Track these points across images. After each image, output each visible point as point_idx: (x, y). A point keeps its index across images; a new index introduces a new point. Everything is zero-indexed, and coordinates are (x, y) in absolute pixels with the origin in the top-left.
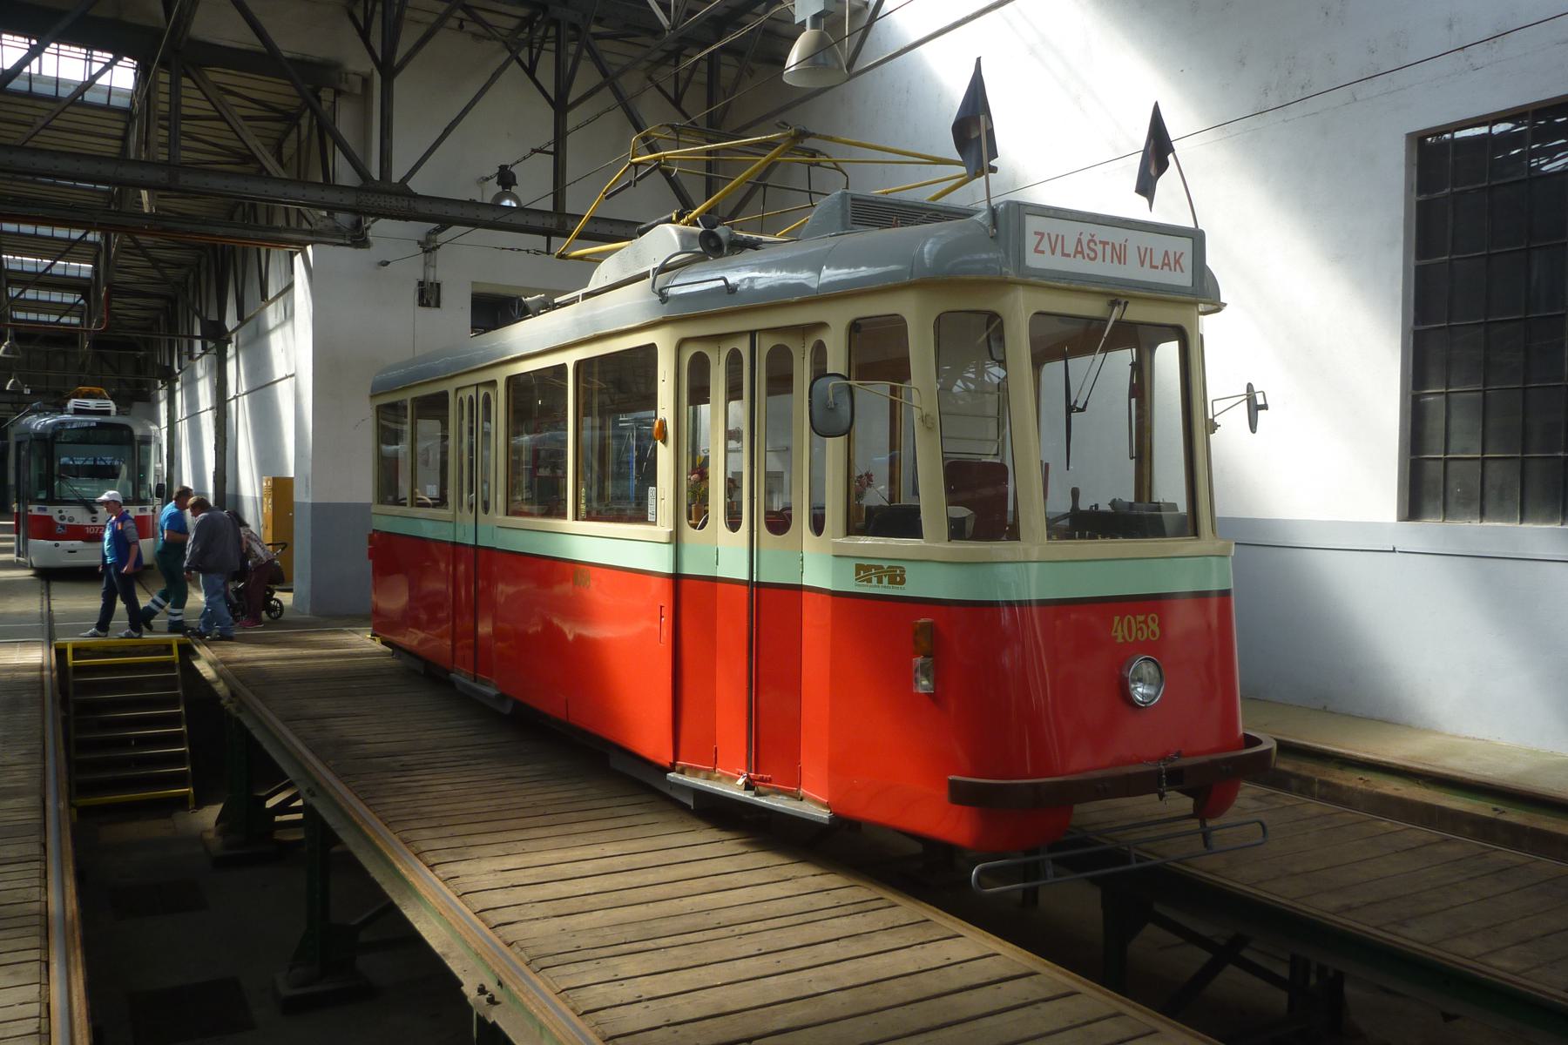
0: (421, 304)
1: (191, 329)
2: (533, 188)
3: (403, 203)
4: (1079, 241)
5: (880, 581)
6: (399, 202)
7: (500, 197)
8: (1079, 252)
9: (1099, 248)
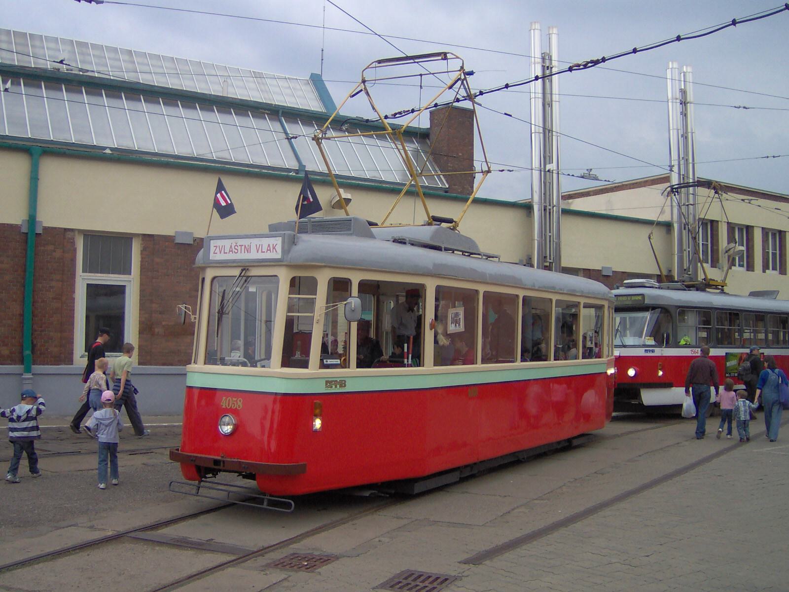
4: (231, 246)
5: (336, 387)
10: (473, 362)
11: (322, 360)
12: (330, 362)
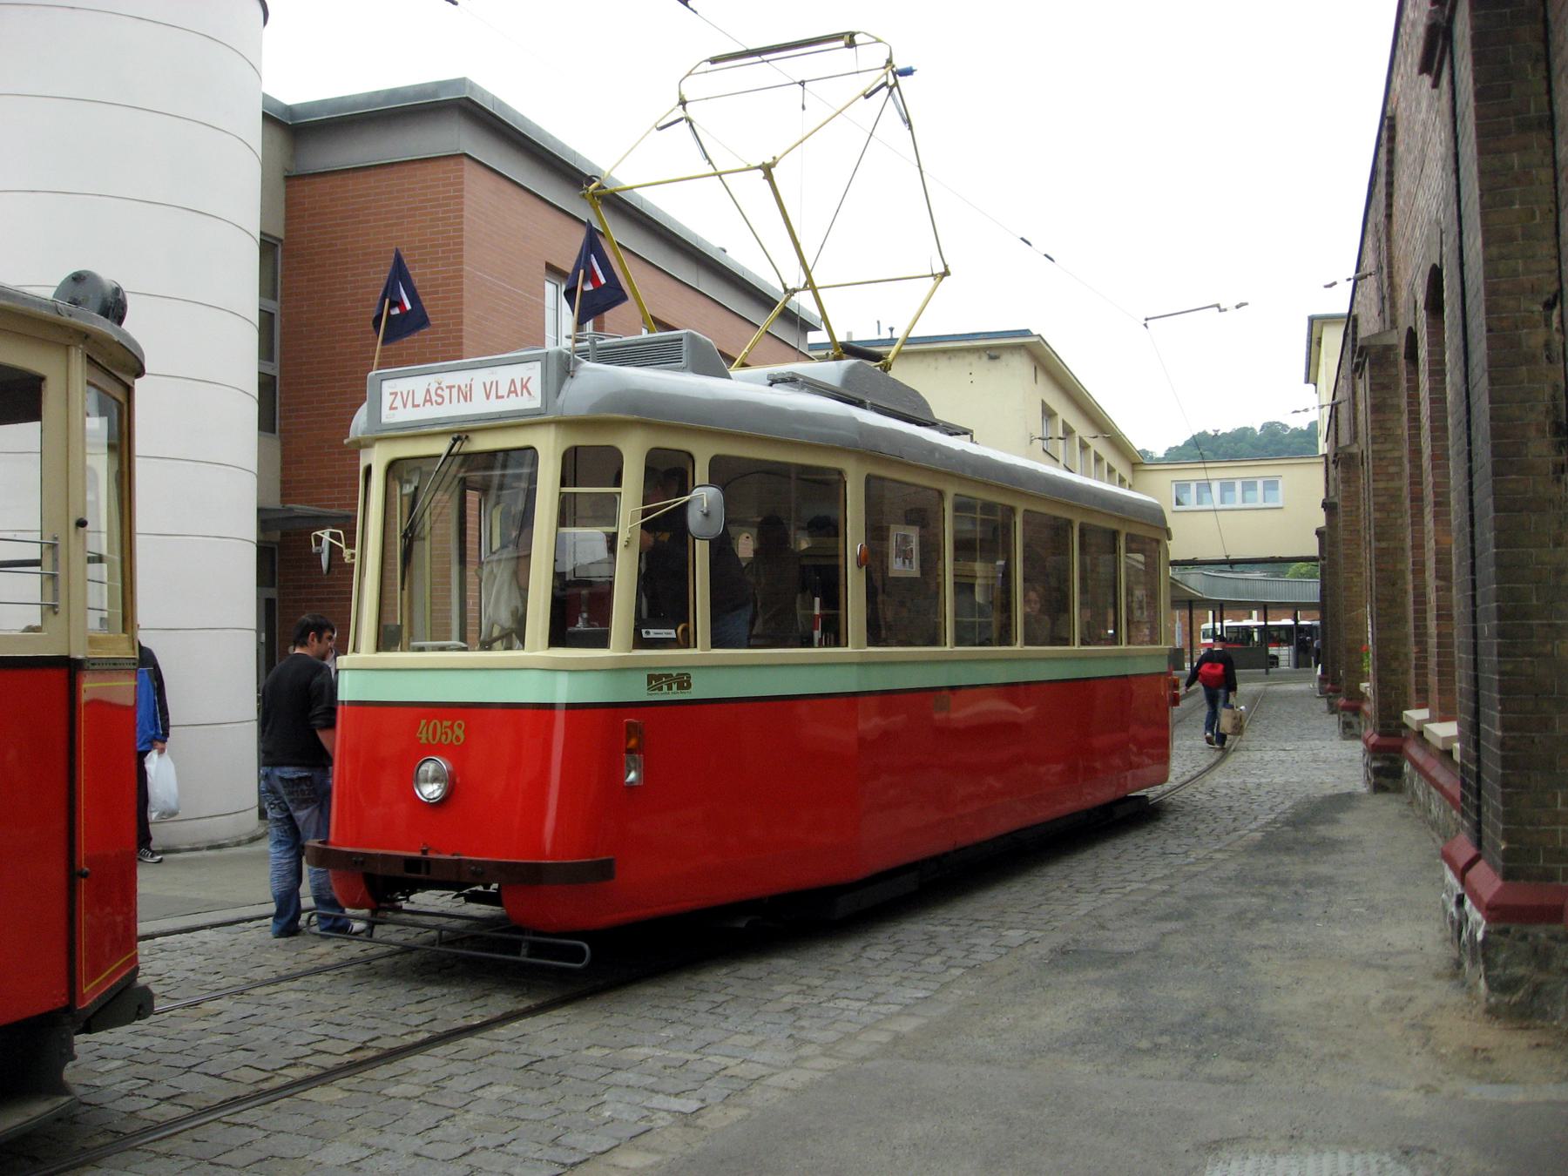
5: (670, 688)
8: (512, 391)
9: (446, 394)
10: (934, 639)
11: (637, 631)
12: (654, 633)
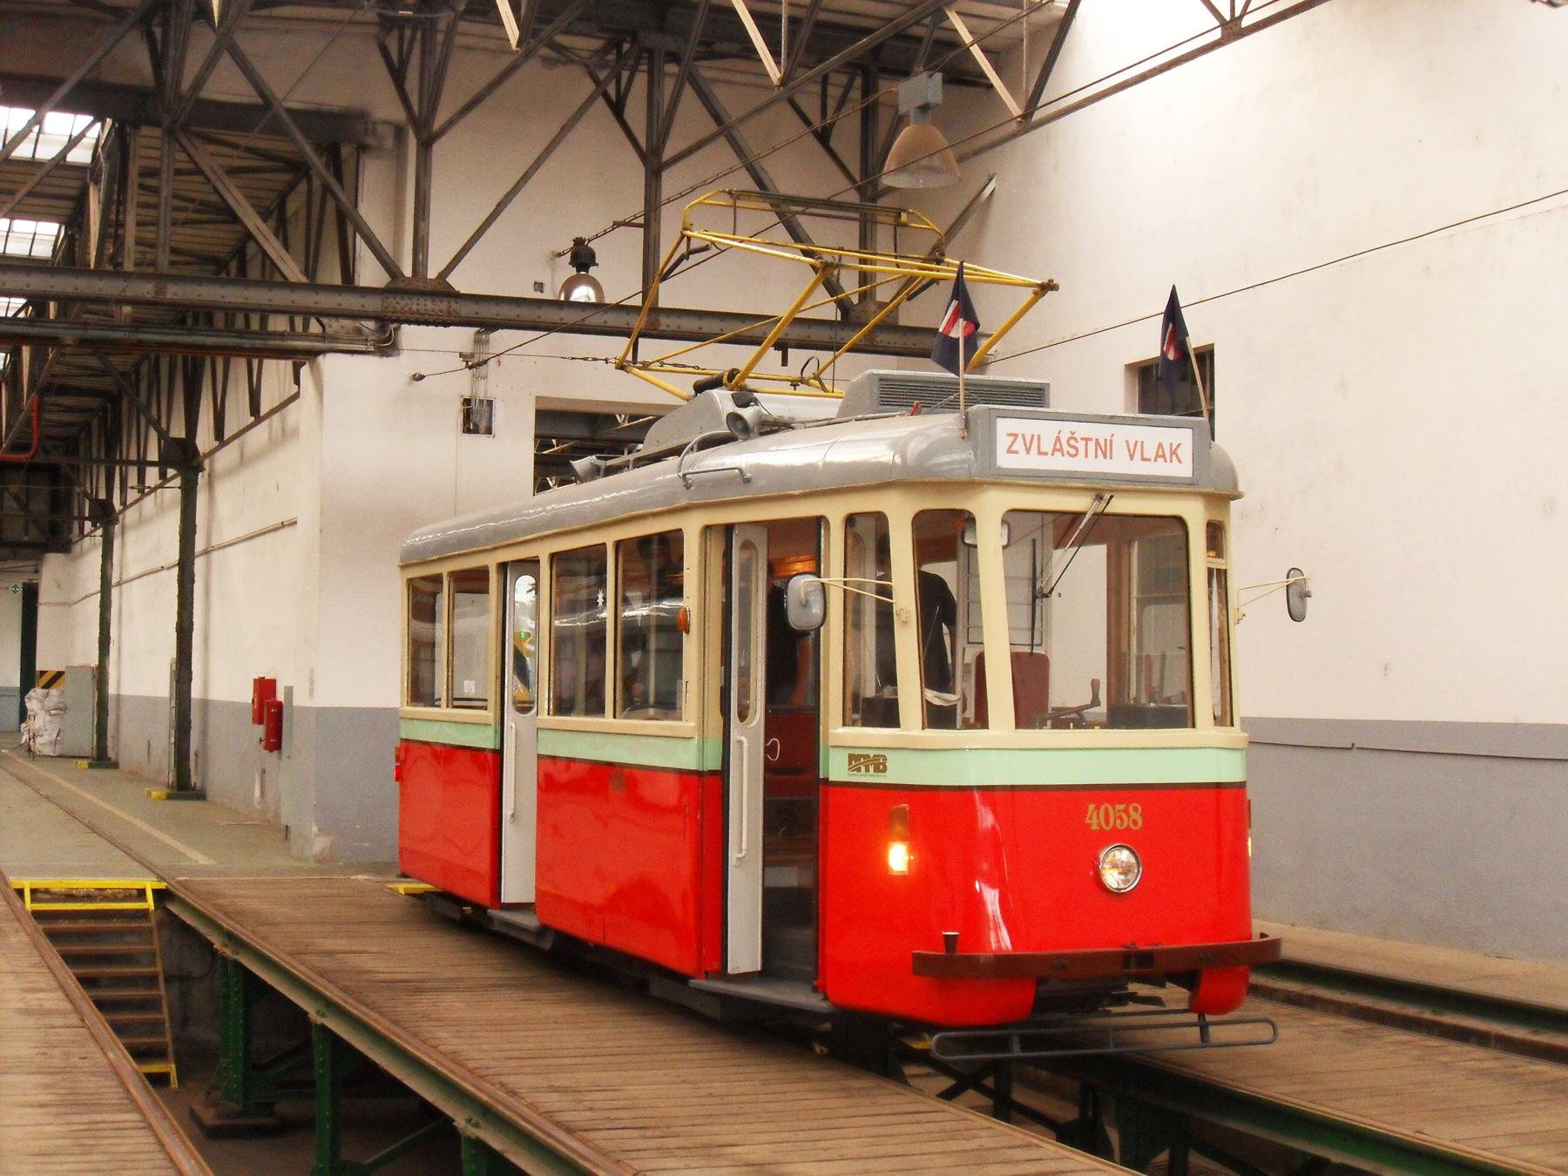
0: (467, 430)
1: (142, 448)
2: (618, 276)
3: (441, 306)
4: (1058, 439)
6: (440, 303)
7: (569, 286)
8: (1160, 455)
